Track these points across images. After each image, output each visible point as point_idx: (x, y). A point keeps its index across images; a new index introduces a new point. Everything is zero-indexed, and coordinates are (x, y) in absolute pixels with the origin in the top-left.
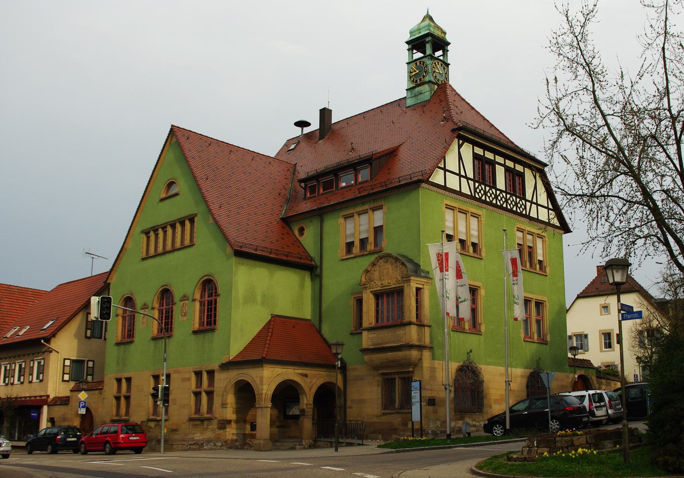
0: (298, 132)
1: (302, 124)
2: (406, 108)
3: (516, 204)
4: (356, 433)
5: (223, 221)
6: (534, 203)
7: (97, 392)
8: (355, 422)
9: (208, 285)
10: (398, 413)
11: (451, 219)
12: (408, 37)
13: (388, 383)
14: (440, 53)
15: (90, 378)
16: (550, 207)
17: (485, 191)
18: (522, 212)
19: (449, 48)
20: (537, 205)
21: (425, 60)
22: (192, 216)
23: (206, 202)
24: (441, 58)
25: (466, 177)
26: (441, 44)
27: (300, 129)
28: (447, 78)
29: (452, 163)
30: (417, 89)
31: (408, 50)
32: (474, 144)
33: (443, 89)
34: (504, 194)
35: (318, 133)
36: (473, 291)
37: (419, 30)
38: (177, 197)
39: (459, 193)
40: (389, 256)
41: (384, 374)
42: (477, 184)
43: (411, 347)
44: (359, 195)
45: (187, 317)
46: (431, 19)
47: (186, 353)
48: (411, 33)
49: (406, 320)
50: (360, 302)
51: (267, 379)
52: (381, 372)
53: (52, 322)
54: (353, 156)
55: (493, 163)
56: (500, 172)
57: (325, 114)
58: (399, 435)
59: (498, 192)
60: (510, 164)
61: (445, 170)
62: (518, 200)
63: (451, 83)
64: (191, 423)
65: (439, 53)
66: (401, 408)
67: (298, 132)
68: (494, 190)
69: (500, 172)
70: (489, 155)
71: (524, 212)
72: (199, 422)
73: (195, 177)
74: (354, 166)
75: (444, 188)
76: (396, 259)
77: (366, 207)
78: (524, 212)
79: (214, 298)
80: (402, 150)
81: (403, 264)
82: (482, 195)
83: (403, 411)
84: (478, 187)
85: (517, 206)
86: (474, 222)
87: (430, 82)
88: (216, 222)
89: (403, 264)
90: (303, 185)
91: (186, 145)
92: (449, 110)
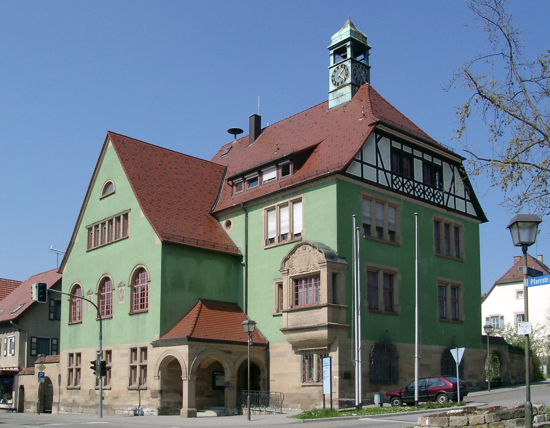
1: (235, 131)
3: (434, 196)
6: (452, 195)
8: (274, 394)
14: (362, 57)
16: (468, 198)
17: (402, 183)
19: (370, 51)
20: (455, 196)
22: (127, 212)
24: (363, 62)
25: (383, 169)
27: (233, 135)
29: (370, 156)
32: (392, 138)
34: (422, 186)
39: (377, 185)
42: (394, 177)
50: (280, 286)
55: (411, 157)
58: (316, 405)
59: (416, 184)
60: (427, 158)
61: (362, 163)
62: (436, 191)
68: (412, 182)
70: (407, 149)
71: (442, 203)
78: (442, 203)
82: (400, 187)
84: (395, 179)
86: (391, 213)
90: (230, 182)
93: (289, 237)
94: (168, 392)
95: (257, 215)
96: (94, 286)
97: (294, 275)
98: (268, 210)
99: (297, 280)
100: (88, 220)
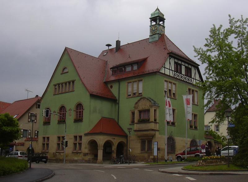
0: (107, 48)
1: (109, 45)
2: (149, 42)
4: (129, 159)
5: (85, 83)
7: (35, 142)
9: (79, 106)
10: (147, 153)
11: (166, 85)
12: (150, 16)
13: (143, 143)
15: (29, 136)
16: (200, 80)
18: (183, 80)
20: (196, 80)
21: (157, 25)
23: (79, 76)
24: (162, 25)
26: (162, 19)
27: (108, 47)
28: (164, 32)
29: (167, 65)
30: (154, 36)
31: (150, 21)
32: (175, 58)
33: (162, 37)
34: (184, 76)
35: (115, 50)
36: (174, 110)
37: (154, 14)
38: (68, 73)
39: (169, 76)
40: (145, 98)
41: (141, 139)
43: (153, 130)
44: (133, 75)
45: (70, 117)
46: (159, 10)
47: (70, 130)
48: (151, 15)
49: (228, 153)
50: (133, 113)
51: (101, 140)
52: (140, 138)
53: (16, 116)
54: (129, 60)
55: (181, 65)
56: (183, 68)
57: (118, 42)
60: (187, 65)
61: (165, 68)
63: (165, 34)
64: (73, 154)
65: (161, 23)
66: (148, 151)
67: (107, 48)
68: (181, 75)
69: (183, 68)
70: (180, 62)
72: (76, 154)
73: (75, 67)
74: (131, 64)
75: (164, 74)
76: (148, 99)
77: (136, 80)
79: (81, 110)
80: (148, 59)
81: (150, 101)
83: (148, 152)
85: (178, 75)
86: (174, 86)
87: (158, 34)
88: (83, 83)
89: (150, 101)
90: (112, 70)
91: (71, 54)
92: (166, 45)
93: (137, 94)
94: (90, 154)
95: (124, 85)
96: (57, 110)
97: (140, 109)
98: (129, 83)
99: (140, 112)
100: (55, 82)
